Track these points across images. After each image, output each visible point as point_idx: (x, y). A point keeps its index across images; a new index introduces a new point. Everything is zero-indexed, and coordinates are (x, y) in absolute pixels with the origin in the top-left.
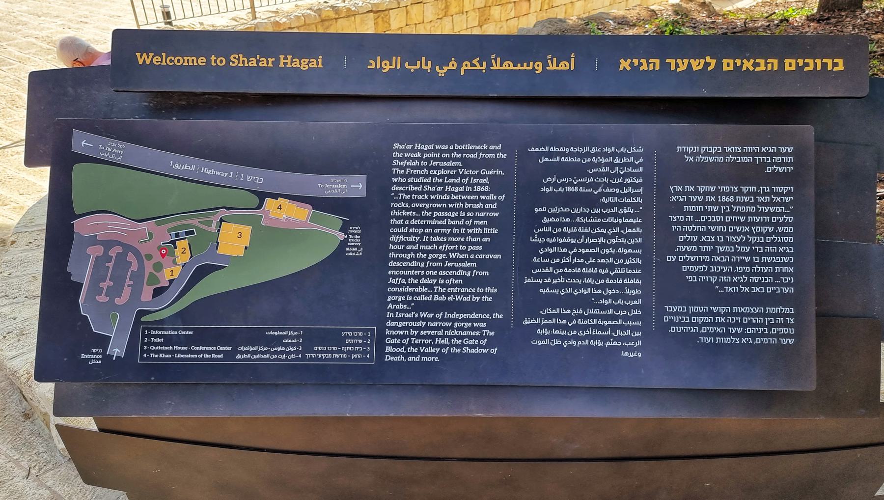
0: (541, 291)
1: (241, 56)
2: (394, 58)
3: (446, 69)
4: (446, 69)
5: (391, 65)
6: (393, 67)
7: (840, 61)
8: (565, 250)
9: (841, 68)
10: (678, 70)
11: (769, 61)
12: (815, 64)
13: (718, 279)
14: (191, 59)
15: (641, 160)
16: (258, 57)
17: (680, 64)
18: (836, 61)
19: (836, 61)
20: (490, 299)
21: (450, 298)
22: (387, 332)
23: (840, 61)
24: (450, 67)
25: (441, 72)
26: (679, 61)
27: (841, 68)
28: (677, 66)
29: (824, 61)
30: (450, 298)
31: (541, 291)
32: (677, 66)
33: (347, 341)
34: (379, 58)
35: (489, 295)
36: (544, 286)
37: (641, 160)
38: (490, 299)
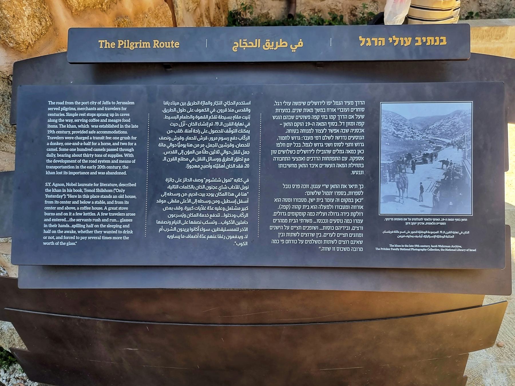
0: (168, 237)
1: (106, 41)
2: (256, 40)
3: (296, 46)
4: (296, 46)
5: (254, 45)
6: (256, 46)
7: (444, 38)
8: (233, 195)
9: (444, 43)
10: (405, 45)
11: (380, 39)
12: (400, 41)
13: (307, 214)
14: (146, 43)
15: (249, 124)
16: (394, 37)
17: (406, 41)
18: (441, 38)
19: (441, 38)
20: (128, 238)
21: (57, 244)
22: (362, 228)
23: (444, 38)
24: (299, 46)
25: (294, 49)
26: (406, 39)
27: (444, 43)
28: (405, 42)
29: (373, 39)
30: (57, 244)
31: (168, 237)
32: (405, 42)
33: (128, 226)
34: (281, 40)
35: (127, 235)
36: (171, 233)
37: (249, 124)
38: (128, 238)
